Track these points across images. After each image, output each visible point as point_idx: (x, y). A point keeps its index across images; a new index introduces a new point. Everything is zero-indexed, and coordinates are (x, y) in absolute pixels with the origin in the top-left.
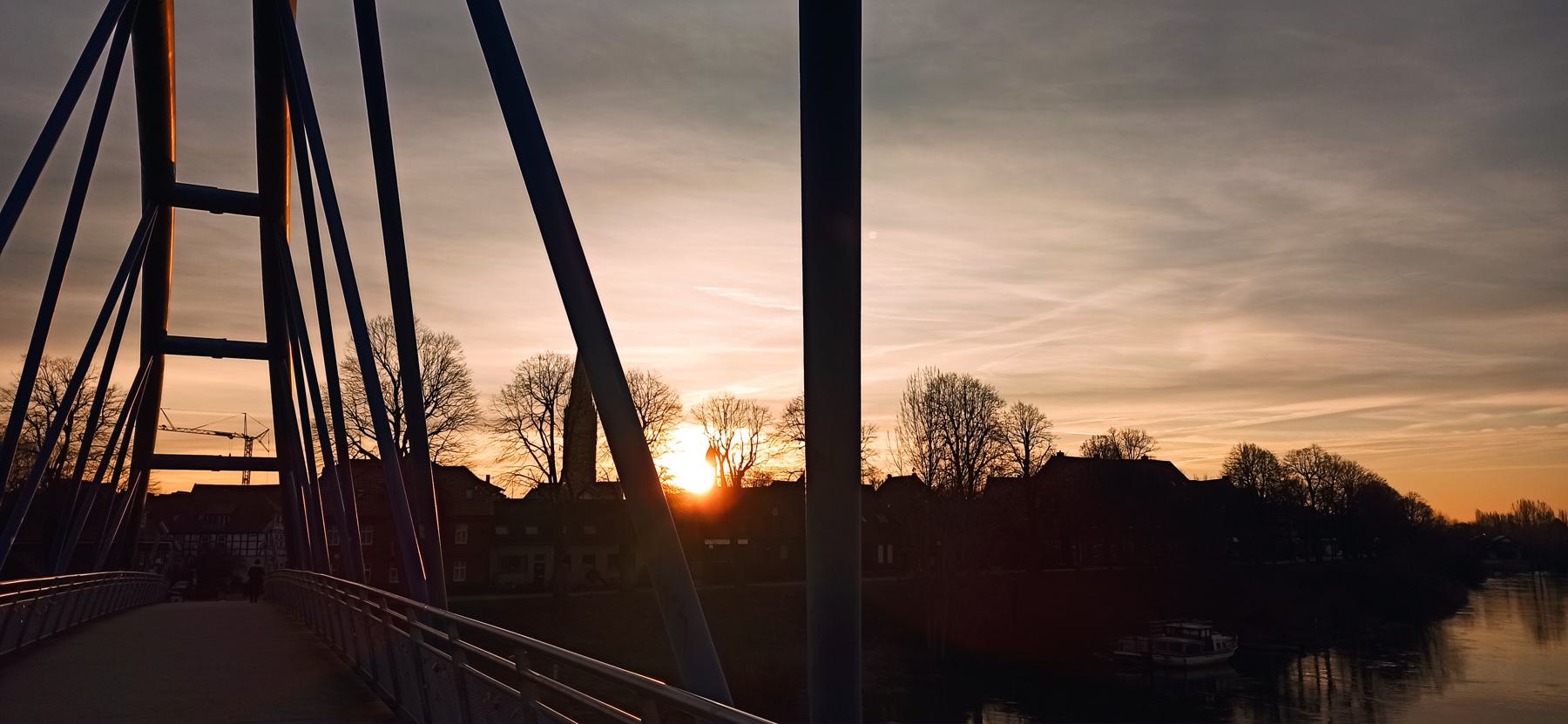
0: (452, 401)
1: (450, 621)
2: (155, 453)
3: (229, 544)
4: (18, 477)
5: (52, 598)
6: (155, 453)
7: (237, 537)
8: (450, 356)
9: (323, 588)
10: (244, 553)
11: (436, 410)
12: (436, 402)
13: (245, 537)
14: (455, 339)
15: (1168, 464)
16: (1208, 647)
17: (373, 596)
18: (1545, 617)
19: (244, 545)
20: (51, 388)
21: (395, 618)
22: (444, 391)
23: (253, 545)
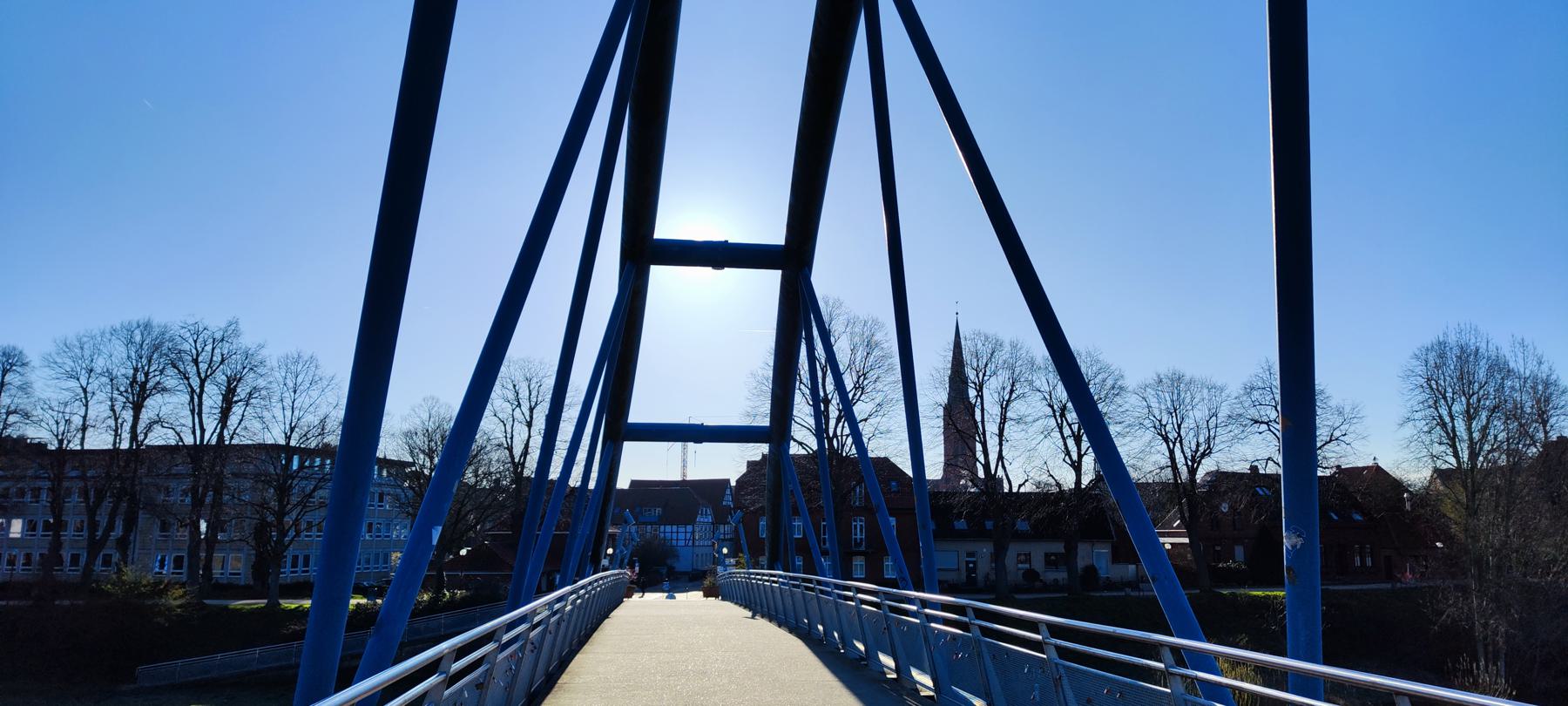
0: (879, 385)
1: (830, 583)
2: (630, 421)
3: (662, 535)
4: (275, 523)
5: (522, 648)
6: (630, 421)
7: (668, 528)
8: (875, 338)
9: (749, 578)
10: (674, 542)
11: (863, 396)
12: (863, 389)
13: (675, 527)
14: (880, 320)
15: (886, 460)
16: (1255, 518)
17: (805, 580)
18: (181, 536)
19: (675, 535)
20: (514, 386)
21: (793, 585)
22: (872, 375)
23: (681, 536)
